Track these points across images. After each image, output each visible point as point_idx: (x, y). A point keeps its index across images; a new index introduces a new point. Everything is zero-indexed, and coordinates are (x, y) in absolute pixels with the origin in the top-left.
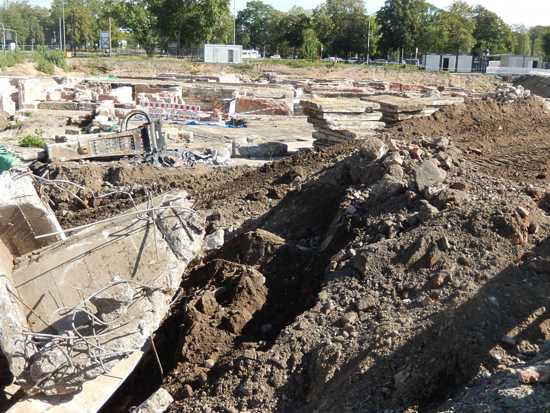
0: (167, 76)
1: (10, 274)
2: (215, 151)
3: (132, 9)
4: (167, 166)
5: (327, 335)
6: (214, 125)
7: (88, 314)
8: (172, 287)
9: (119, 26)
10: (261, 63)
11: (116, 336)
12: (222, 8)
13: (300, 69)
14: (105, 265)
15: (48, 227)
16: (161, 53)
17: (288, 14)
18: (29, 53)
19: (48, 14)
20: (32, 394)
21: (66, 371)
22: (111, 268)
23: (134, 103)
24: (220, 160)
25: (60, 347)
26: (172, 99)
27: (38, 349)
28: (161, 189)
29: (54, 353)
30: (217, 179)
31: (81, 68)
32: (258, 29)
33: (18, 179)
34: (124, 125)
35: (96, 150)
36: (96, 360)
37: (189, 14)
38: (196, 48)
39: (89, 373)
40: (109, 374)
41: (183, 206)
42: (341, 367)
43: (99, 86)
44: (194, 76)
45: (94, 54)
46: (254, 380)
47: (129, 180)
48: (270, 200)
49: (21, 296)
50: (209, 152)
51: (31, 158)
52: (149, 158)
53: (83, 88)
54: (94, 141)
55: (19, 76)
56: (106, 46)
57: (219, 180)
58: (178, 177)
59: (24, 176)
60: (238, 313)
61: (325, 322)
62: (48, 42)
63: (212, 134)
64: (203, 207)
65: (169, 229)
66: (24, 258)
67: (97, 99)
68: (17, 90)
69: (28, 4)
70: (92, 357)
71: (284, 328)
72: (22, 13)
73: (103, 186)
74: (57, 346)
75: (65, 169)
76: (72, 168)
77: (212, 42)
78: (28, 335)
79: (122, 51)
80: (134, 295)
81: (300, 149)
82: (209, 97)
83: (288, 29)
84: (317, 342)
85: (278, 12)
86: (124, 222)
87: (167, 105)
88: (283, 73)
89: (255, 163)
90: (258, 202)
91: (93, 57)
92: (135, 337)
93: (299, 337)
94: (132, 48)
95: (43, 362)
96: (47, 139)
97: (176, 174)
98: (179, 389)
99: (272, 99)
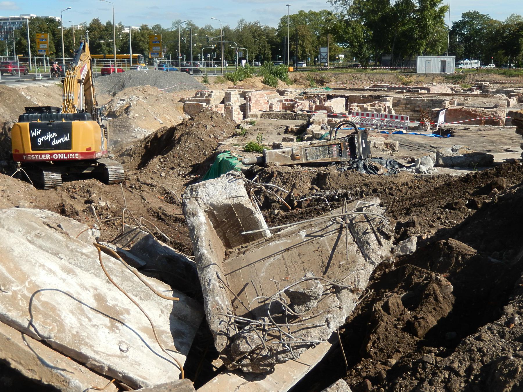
0: (379, 87)
1: (221, 263)
2: (418, 160)
3: (350, 25)
4: (372, 173)
5: (509, 349)
6: (421, 134)
7: (282, 304)
8: (359, 287)
9: (337, 42)
10: (474, 72)
11: (305, 327)
12: (437, 20)
13: (516, 78)
14: (301, 262)
15: (256, 224)
16: (375, 65)
17: (505, 23)
18: (257, 69)
19: (275, 33)
20: (231, 369)
21: (260, 352)
22: (305, 265)
23: (346, 112)
24: (424, 168)
25: (257, 331)
26: (383, 109)
27: (239, 331)
28: (364, 195)
29: (251, 336)
30: (418, 187)
31: (301, 81)
32: (473, 39)
33: (232, 181)
34: (334, 134)
35: (307, 156)
36: (286, 346)
37: (404, 28)
38: (409, 60)
39: (280, 356)
40: (297, 360)
41: (375, 212)
42: (520, 382)
43: (316, 97)
44: (405, 86)
45: (314, 68)
46: (431, 383)
47: (335, 185)
48: (470, 210)
49: (229, 283)
50: (413, 160)
51: (251, 162)
52: (354, 166)
53: (302, 99)
54: (305, 148)
55: (248, 89)
56: (324, 61)
57: (419, 189)
58: (381, 184)
59: (238, 179)
60: (423, 318)
61: (508, 335)
62: (274, 58)
63: (418, 143)
64: (402, 214)
65: (360, 233)
66: (234, 250)
67: (314, 110)
68: (245, 102)
69: (259, 25)
70: (284, 342)
71: (465, 337)
72: (253, 33)
73: (311, 189)
74: (254, 330)
75: (279, 173)
76: (285, 172)
77: (425, 53)
78: (231, 317)
79: (339, 65)
80: (324, 292)
81: (506, 160)
82: (419, 107)
83: (503, 38)
84: (498, 355)
85: (495, 22)
86: (320, 224)
87: (377, 115)
88: (497, 83)
89: (457, 173)
90: (457, 211)
91: (312, 71)
92: (322, 330)
93: (480, 348)
94: (348, 61)
95: (241, 342)
96: (266, 145)
97: (379, 181)
98: (360, 383)
99: (483, 109)
